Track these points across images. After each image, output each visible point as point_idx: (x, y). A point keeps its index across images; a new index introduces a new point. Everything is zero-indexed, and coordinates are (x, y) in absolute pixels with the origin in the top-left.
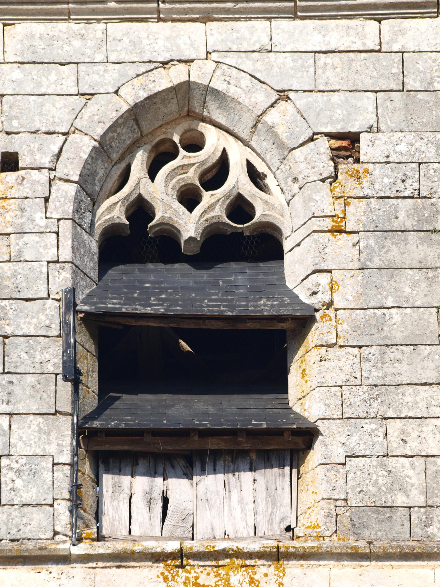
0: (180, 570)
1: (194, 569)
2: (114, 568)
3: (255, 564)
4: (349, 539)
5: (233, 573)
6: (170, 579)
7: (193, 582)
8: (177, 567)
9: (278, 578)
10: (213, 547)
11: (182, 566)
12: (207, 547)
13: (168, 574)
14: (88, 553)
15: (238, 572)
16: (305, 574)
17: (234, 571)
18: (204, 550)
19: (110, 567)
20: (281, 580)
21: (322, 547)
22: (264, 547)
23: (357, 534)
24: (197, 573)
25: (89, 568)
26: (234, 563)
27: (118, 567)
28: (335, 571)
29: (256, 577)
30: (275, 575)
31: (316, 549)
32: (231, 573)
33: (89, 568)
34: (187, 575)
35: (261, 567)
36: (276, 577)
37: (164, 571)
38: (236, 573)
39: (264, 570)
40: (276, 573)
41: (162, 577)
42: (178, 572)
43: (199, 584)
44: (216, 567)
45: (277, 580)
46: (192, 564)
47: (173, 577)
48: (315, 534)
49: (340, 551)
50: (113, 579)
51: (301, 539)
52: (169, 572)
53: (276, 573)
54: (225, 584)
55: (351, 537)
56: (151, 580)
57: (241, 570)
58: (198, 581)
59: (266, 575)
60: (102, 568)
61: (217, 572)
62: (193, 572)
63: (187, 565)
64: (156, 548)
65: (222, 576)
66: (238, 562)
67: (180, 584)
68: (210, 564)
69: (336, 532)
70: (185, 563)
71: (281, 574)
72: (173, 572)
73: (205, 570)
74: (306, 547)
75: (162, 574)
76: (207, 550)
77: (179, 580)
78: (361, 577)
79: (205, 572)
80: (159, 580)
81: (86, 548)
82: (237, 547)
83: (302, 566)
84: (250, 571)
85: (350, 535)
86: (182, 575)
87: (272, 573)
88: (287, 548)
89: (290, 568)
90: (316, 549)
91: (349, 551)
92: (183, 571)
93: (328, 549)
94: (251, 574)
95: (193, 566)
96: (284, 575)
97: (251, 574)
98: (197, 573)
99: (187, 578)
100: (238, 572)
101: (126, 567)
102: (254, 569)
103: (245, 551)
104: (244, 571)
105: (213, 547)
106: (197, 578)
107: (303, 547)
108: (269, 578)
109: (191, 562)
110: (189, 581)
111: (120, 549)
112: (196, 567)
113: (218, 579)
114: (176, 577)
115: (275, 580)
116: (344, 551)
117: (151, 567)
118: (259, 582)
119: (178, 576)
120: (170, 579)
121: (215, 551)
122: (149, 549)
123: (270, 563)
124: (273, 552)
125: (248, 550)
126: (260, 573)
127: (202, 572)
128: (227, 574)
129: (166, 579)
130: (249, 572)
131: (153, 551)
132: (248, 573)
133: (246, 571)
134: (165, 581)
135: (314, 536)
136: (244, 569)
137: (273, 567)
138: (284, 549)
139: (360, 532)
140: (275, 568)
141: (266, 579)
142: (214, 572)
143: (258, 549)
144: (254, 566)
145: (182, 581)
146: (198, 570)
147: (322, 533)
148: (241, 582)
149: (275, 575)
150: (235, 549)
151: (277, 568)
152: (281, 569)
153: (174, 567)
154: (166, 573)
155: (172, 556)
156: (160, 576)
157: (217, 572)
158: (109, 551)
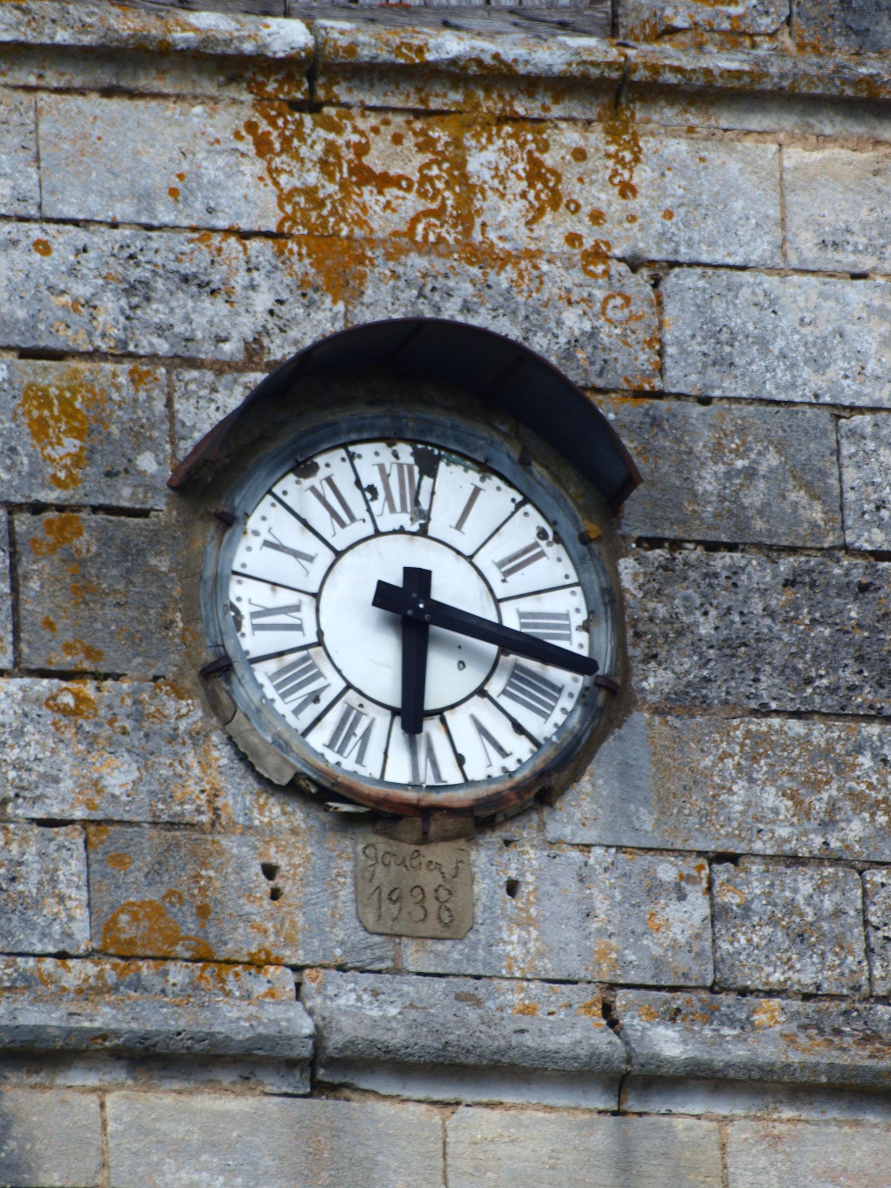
0: (308, 119)
1: (351, 118)
2: (94, 97)
3: (543, 114)
4: (832, 49)
5: (473, 143)
6: (277, 146)
7: (349, 162)
8: (296, 106)
9: (619, 167)
10: (420, 50)
11: (313, 106)
12: (399, 47)
13: (270, 129)
14: (22, 38)
15: (490, 140)
16: (702, 160)
17: (477, 136)
18: (392, 57)
19: (81, 92)
20: (626, 174)
21: (767, 74)
22: (584, 62)
23: (857, 33)
24: (362, 133)
25: (16, 88)
26: (478, 105)
27: (108, 92)
28: (795, 155)
29: (549, 159)
30: (608, 156)
31: (746, 79)
32: (469, 141)
33: (16, 88)
34: (332, 136)
35: (563, 125)
36: (611, 163)
37: (256, 118)
38: (484, 140)
39: (572, 137)
40: (612, 148)
41: (249, 138)
42: (300, 124)
43: (369, 170)
44: (417, 114)
45: (615, 173)
46: (344, 98)
47: (286, 141)
48: (726, 25)
49: (819, 91)
50: (97, 132)
51: (680, 37)
52: (273, 122)
53: (612, 148)
54: (450, 174)
55: (839, 41)
56: (217, 147)
57: (498, 134)
58: (366, 160)
59: (580, 155)
60: (58, 91)
61: (424, 133)
62: (349, 128)
63: (329, 103)
64: (241, 39)
65: (440, 147)
66: (490, 103)
67: (309, 165)
68: (400, 105)
69: (789, 21)
70: (321, 94)
71: (628, 156)
72: (286, 122)
73: (386, 123)
74: (716, 72)
75: (251, 127)
76: (401, 61)
77: (304, 151)
78: (879, 180)
79: (387, 132)
80: (241, 146)
81: (13, 21)
82: (496, 56)
83: (691, 130)
84: (530, 137)
85: (836, 34)
86: (314, 136)
87: (597, 150)
88: (655, 69)
89: (652, 134)
90: (746, 79)
91: (849, 91)
92: (316, 124)
93: (785, 84)
94: (532, 146)
95: (348, 106)
96: (637, 160)
97: (532, 146)
98: (362, 133)
99: (331, 148)
100: (490, 140)
101: (133, 94)
102: (541, 132)
103: (521, 69)
104: (510, 136)
105: (420, 50)
106: (362, 150)
107: (708, 72)
108: (589, 164)
109: (341, 92)
110: (338, 157)
111: (125, 34)
112: (355, 111)
113: (429, 156)
114: (296, 142)
115: (609, 173)
116: (834, 91)
117: (215, 100)
118: (559, 177)
119: (303, 140)
120: (277, 146)
121: (427, 64)
122: (217, 42)
123: (592, 114)
124: (609, 80)
125: (530, 68)
126: (562, 145)
127: (375, 130)
128: (457, 142)
129: (263, 146)
130: (525, 142)
131: (231, 51)
132: (522, 145)
133: (514, 136)
134: (260, 154)
135: (722, 32)
136: (508, 129)
137: (598, 127)
138: (647, 73)
139: (865, 24)
140: (607, 132)
141: (578, 168)
142: (415, 134)
143: (564, 67)
144: (540, 120)
145: (315, 158)
146: (361, 124)
147: (748, 20)
148: (502, 172)
149: (608, 156)
150: (488, 59)
151: (613, 134)
152: (626, 137)
153: (285, 107)
154: (264, 126)
155: (291, 67)
156: (244, 133)
157: (424, 133)
158: (87, 40)
